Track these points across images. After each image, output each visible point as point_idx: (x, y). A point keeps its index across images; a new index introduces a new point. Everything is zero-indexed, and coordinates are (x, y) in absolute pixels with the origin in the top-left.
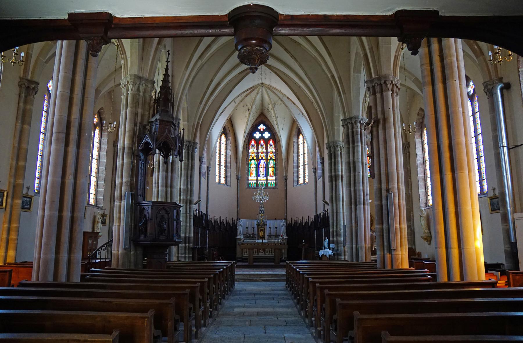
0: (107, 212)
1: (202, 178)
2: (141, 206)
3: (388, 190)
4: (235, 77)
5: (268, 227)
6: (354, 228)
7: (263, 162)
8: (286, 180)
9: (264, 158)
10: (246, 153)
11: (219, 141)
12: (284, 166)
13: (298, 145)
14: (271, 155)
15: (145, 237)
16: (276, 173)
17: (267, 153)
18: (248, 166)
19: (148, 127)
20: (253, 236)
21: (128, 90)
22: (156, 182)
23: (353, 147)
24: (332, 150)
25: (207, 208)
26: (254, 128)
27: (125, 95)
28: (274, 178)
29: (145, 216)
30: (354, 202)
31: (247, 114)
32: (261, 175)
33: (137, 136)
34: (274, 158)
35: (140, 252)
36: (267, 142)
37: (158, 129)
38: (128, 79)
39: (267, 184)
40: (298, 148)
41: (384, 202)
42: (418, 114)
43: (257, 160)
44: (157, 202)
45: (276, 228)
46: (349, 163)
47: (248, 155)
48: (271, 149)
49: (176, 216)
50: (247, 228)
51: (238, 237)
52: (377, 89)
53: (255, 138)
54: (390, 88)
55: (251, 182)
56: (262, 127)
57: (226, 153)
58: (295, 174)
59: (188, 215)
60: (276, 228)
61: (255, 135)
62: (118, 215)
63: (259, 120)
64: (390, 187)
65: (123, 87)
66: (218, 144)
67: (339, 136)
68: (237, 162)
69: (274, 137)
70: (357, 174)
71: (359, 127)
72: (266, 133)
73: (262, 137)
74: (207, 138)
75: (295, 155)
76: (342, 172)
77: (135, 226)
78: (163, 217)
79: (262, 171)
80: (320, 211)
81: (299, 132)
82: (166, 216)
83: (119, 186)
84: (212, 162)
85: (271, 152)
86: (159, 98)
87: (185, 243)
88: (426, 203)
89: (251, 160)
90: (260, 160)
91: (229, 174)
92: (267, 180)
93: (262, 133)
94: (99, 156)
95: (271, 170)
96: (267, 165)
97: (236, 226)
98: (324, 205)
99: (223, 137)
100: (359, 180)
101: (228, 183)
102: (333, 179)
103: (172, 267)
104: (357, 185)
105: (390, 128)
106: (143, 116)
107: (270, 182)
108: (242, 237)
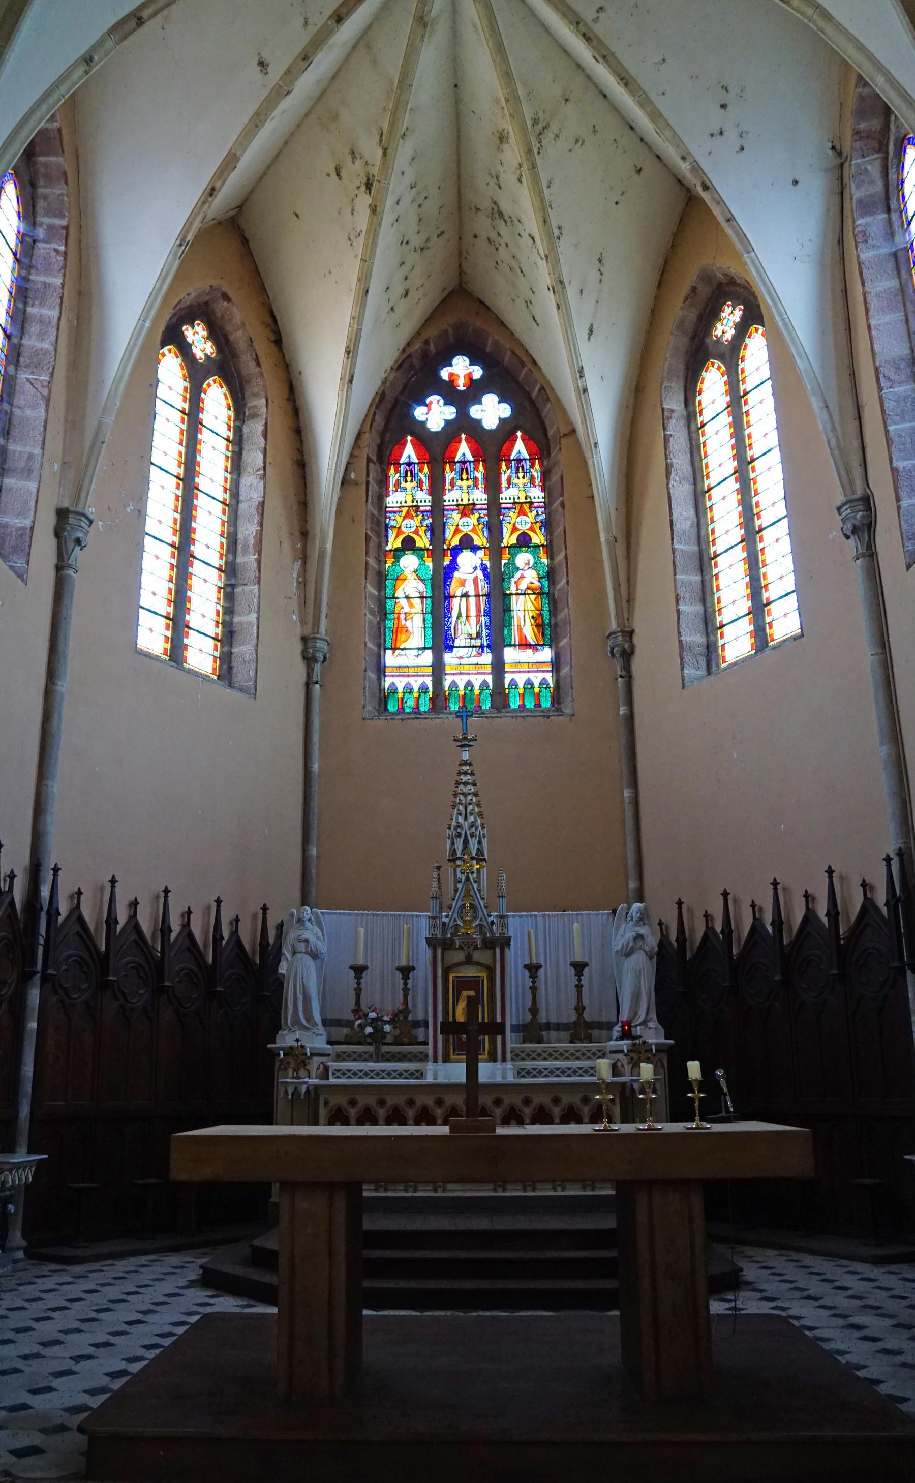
5: (515, 958)
8: (627, 655)
10: (363, 509)
12: (611, 567)
14: (524, 523)
16: (554, 626)
17: (495, 508)
18: (381, 586)
20: (396, 1033)
25: (39, 809)
26: (416, 374)
28: (546, 654)
31: (362, 219)
32: (457, 643)
34: (538, 538)
36: (492, 449)
39: (499, 695)
40: (695, 450)
45: (579, 967)
47: (380, 524)
48: (521, 488)
50: (359, 971)
51: (286, 1039)
53: (420, 433)
55: (400, 683)
56: (461, 369)
57: (234, 490)
58: (691, 609)
60: (579, 967)
61: (419, 413)
63: (446, 323)
67: (512, 1190)
68: (304, 558)
69: (540, 421)
72: (490, 399)
73: (464, 425)
75: (681, 491)
79: (467, 620)
85: (521, 507)
89: (398, 553)
90: (455, 552)
91: (246, 619)
92: (498, 667)
93: (463, 399)
95: (523, 611)
96: (497, 579)
101: (242, 674)
107: (521, 679)
108: (316, 1041)
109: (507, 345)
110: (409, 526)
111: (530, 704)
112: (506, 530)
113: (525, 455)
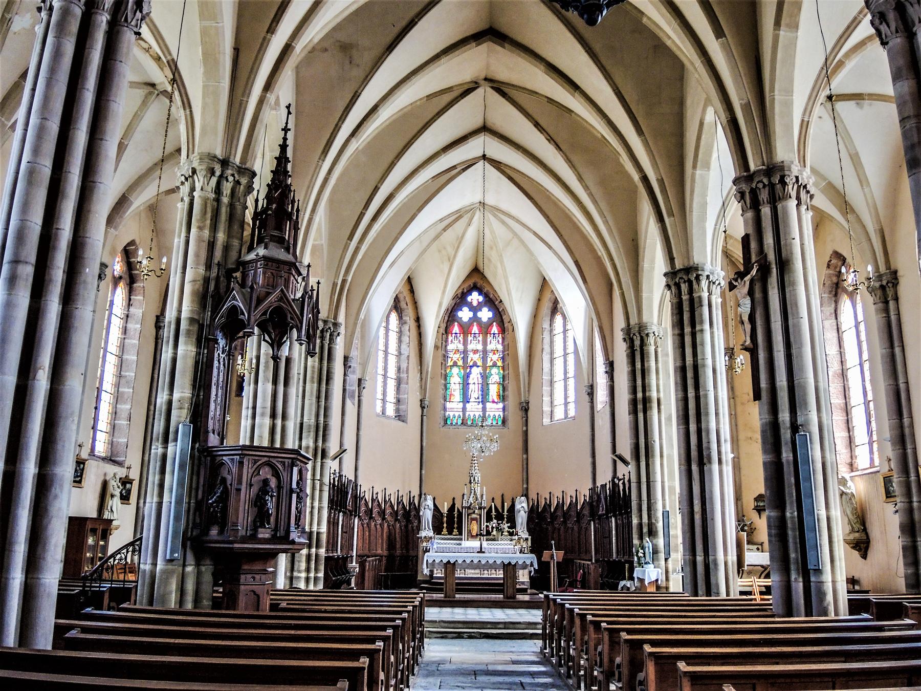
0: (135, 475)
1: (348, 402)
2: (213, 457)
3: (795, 428)
4: (425, 185)
6: (698, 517)
7: (476, 372)
9: (480, 363)
11: (384, 324)
13: (552, 336)
14: (495, 358)
15: (221, 532)
17: (485, 352)
18: (446, 379)
19: (238, 275)
21: (193, 189)
22: (251, 405)
23: (693, 335)
24: (637, 343)
26: (460, 300)
27: (187, 199)
29: (224, 480)
30: (696, 458)
33: (211, 296)
34: (500, 364)
35: (207, 570)
36: (485, 329)
37: (260, 280)
38: (196, 164)
40: (552, 342)
41: (786, 455)
42: (828, 266)
43: (465, 367)
44: (251, 447)
46: (682, 370)
47: (445, 357)
48: (495, 344)
49: (298, 483)
51: (423, 534)
52: (764, 195)
54: (794, 194)
55: (451, 414)
56: (475, 298)
59: (318, 483)
61: (460, 314)
62: (157, 477)
63: (470, 282)
64: (800, 420)
65: (182, 183)
66: (382, 331)
69: (501, 318)
70: (701, 393)
71: (706, 289)
72: (485, 309)
73: (475, 319)
74: (362, 316)
76: (658, 391)
77: (199, 504)
78: (266, 482)
79: (475, 392)
80: (604, 477)
81: (555, 308)
82: (273, 483)
83: (164, 408)
84: (370, 368)
85: (494, 352)
86: (264, 210)
87: (310, 546)
88: (851, 465)
90: (471, 367)
93: (475, 309)
94: (122, 347)
95: (494, 390)
96: (485, 377)
97: (418, 510)
98: (615, 462)
99: (394, 316)
100: (707, 408)
102: (640, 407)
103: (284, 605)
104: (703, 418)
105: (793, 284)
106: (227, 248)
107: (492, 414)
109: (490, 291)
110: (456, 357)
111: (494, 423)
112: (489, 360)
113: (496, 332)
